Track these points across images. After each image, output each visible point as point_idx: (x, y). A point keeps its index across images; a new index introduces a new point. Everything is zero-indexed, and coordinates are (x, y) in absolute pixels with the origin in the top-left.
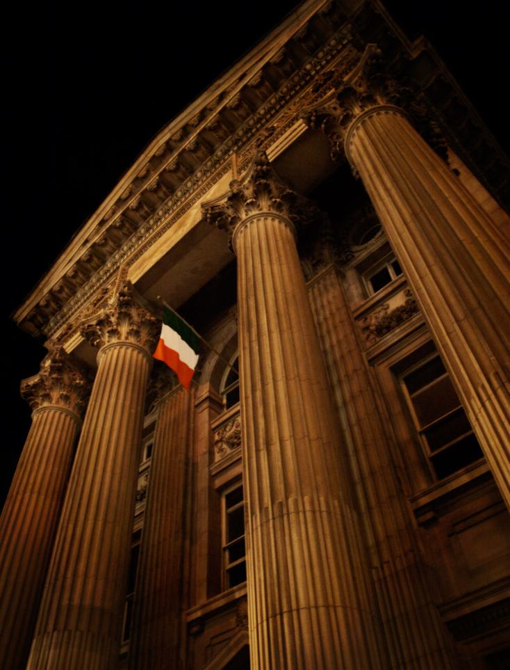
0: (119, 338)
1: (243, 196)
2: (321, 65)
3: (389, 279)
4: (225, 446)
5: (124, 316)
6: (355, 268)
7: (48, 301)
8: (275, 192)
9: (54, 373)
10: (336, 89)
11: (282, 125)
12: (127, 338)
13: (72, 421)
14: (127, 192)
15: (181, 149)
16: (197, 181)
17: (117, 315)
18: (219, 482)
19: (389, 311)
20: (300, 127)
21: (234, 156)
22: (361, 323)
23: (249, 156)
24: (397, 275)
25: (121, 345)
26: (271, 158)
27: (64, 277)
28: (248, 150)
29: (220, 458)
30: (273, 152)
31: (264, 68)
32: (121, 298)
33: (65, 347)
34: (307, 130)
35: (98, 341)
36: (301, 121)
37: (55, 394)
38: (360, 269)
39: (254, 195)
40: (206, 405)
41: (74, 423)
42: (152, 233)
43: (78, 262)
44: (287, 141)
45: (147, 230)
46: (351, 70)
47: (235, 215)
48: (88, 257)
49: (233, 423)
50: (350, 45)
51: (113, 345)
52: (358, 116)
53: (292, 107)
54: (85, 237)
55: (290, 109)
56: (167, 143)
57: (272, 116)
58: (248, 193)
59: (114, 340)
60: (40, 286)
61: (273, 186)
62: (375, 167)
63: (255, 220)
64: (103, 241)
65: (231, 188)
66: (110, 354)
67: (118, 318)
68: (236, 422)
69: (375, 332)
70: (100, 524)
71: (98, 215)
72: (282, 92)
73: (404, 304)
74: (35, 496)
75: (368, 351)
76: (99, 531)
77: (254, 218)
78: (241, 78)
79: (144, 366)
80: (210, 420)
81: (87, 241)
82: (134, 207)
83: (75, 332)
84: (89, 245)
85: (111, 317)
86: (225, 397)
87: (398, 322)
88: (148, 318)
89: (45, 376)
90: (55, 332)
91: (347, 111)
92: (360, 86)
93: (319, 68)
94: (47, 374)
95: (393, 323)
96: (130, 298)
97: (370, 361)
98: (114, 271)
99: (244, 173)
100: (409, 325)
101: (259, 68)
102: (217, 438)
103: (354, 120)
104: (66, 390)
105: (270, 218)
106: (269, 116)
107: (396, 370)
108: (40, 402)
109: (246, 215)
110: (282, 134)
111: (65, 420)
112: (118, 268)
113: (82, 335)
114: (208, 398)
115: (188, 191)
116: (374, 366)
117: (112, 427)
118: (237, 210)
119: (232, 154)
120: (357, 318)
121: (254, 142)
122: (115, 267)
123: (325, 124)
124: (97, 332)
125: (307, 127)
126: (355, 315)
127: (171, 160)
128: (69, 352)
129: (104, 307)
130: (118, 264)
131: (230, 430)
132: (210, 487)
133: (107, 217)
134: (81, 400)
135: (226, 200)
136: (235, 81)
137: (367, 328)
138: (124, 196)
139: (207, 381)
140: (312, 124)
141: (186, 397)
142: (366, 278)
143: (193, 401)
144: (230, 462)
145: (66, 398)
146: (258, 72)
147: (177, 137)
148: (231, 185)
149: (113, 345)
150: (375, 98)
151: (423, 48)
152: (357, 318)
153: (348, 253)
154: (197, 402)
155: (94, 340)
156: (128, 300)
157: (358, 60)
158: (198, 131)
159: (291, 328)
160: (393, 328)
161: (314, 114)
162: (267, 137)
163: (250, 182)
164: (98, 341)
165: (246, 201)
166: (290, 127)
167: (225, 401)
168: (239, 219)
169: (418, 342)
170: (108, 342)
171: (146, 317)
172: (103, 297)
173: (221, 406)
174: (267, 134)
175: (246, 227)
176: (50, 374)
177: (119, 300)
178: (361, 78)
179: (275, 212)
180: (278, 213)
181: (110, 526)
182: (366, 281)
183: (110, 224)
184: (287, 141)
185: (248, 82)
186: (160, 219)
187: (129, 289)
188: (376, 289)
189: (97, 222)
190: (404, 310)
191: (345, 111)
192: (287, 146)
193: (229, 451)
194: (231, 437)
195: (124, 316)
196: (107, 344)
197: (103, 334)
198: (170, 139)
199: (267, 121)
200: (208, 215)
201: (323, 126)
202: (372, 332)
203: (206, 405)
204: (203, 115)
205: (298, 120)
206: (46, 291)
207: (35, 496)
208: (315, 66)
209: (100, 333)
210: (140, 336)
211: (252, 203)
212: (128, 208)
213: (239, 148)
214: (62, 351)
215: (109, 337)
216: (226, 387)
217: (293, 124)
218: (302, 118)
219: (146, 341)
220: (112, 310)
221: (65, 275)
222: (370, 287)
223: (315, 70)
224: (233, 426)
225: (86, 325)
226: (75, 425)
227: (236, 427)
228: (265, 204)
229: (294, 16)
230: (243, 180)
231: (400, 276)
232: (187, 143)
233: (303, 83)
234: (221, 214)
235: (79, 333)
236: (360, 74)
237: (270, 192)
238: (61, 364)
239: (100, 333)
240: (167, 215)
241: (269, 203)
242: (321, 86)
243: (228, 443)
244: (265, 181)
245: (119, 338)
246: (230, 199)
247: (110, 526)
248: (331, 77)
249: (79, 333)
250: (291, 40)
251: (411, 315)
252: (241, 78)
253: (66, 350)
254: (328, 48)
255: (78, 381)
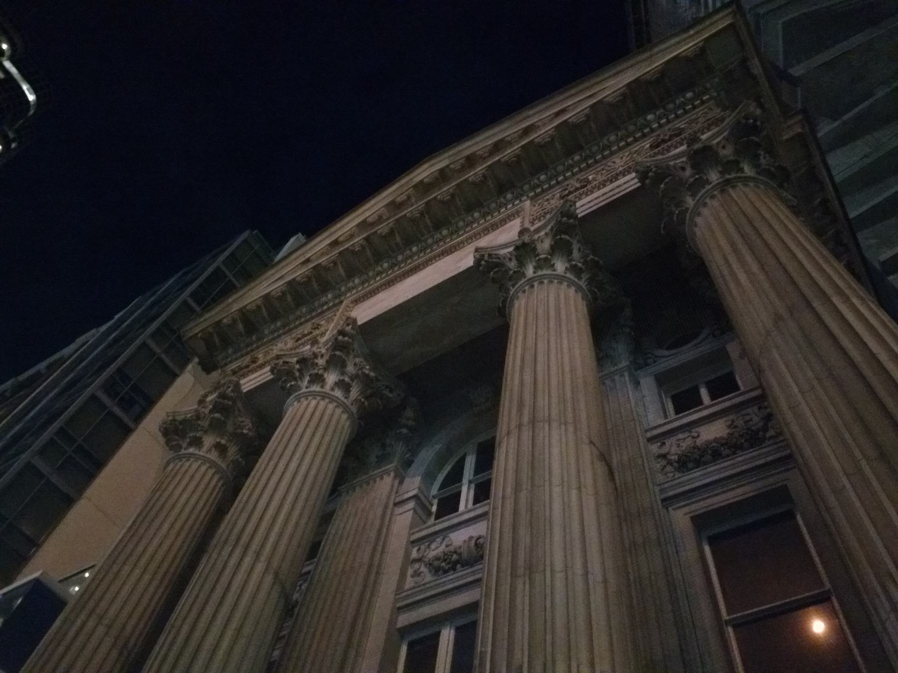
0: (322, 387)
1: (535, 249)
2: (667, 119)
3: (699, 402)
4: (423, 569)
5: (335, 362)
6: (655, 376)
7: (234, 321)
8: (576, 254)
9: (217, 412)
10: (688, 146)
11: (600, 178)
12: (332, 389)
13: (220, 484)
14: (375, 216)
15: (464, 178)
16: (472, 223)
17: (326, 357)
18: (404, 620)
19: (699, 442)
20: (629, 182)
21: (528, 203)
22: (654, 448)
23: (549, 207)
24: (712, 399)
25: (324, 396)
26: (581, 212)
27: (267, 297)
28: (548, 200)
29: (412, 585)
30: (584, 205)
31: (592, 107)
32: (340, 338)
33: (242, 382)
34: (638, 188)
35: (293, 383)
36: (634, 175)
37: (209, 441)
38: (661, 380)
39: (551, 252)
40: (411, 505)
41: (223, 485)
42: (398, 272)
43: (290, 283)
44: (604, 197)
45: (392, 267)
46: (709, 130)
47: (519, 269)
48: (305, 279)
49: (443, 539)
50: (712, 102)
51: (314, 395)
52: (713, 184)
53: (618, 161)
54: (308, 256)
55: (614, 162)
56: (442, 171)
57: (589, 166)
58: (545, 246)
59: (316, 388)
60: (230, 300)
61: (575, 247)
62: (733, 244)
63: (546, 281)
64: (332, 264)
65: (519, 236)
66: (305, 403)
67: (327, 362)
68: (446, 539)
69: (676, 465)
70: (230, 633)
71: (331, 234)
72: (608, 140)
73: (725, 436)
74: (137, 572)
75: (662, 487)
76: (225, 644)
77: (534, 281)
78: (558, 114)
79: (345, 431)
80: (411, 527)
81: (308, 261)
82: (384, 234)
83: (261, 366)
84: (311, 265)
85: (319, 358)
86: (435, 502)
87: (713, 456)
88: (367, 372)
89: (204, 412)
90: (231, 362)
91: (701, 175)
92: (724, 147)
93: (663, 121)
94: (207, 411)
95: (708, 457)
96: (350, 340)
97: (663, 500)
98: (334, 306)
99: (538, 225)
100: (718, 470)
101: (587, 105)
102: (414, 554)
103: (708, 187)
104: (226, 438)
105: (566, 284)
106: (584, 165)
107: (700, 522)
108: (184, 445)
109: (534, 272)
110: (599, 189)
111: (211, 479)
112: (341, 302)
113: (272, 371)
114: (415, 497)
115: (456, 231)
116: (667, 510)
117: (284, 498)
118: (521, 264)
119: (525, 201)
120: (650, 440)
121: (557, 192)
122: (337, 301)
123: (666, 184)
124: (294, 373)
125: (639, 185)
126: (649, 435)
127: (445, 189)
128: (244, 391)
129: (313, 344)
130: (342, 298)
131: (437, 548)
132: (392, 622)
133: (341, 239)
134: (241, 457)
135: (511, 249)
136: (549, 116)
137: (664, 456)
138: (370, 220)
139: (419, 475)
140: (647, 181)
141: (388, 488)
142: (665, 393)
143: (393, 497)
144: (440, 590)
145: (221, 449)
146: (585, 109)
147: (457, 166)
148: (521, 233)
149: (314, 395)
150: (742, 165)
151: (800, 130)
152: (650, 440)
153: (649, 356)
154: (398, 500)
155: (285, 382)
156: (348, 342)
157: (722, 120)
158: (489, 163)
159: (155, 573)
160: (723, 458)
161: (654, 169)
162: (577, 189)
163: (546, 234)
164: (293, 383)
165: (538, 255)
166: (612, 182)
167: (434, 509)
168: (524, 275)
169: (739, 491)
170: (307, 388)
171: (364, 370)
172: (311, 333)
173: (429, 513)
174: (578, 185)
175: (532, 286)
176: (211, 412)
177: (336, 339)
178: (726, 139)
179: (572, 277)
180: (576, 280)
181: (242, 641)
182: (666, 397)
183: (346, 246)
184: (604, 197)
185: (570, 118)
186: (426, 249)
187: (352, 328)
188: (713, 396)
189: (328, 241)
190: (726, 444)
191: (698, 174)
192: (604, 203)
193: (428, 577)
194: (437, 558)
195: (335, 362)
196: (304, 390)
197: (301, 377)
198: (448, 166)
199: (581, 170)
200: (483, 262)
201: (662, 186)
202: (670, 463)
203: (411, 505)
204: (498, 147)
205: (629, 173)
206: (236, 307)
207: (137, 572)
208: (660, 118)
209: (297, 374)
210: (349, 391)
211: (546, 259)
212: (375, 232)
213: (537, 195)
214: (237, 386)
215: (309, 382)
216: (440, 489)
217: (617, 179)
218: (637, 172)
219: (356, 400)
220: (323, 351)
221: (270, 293)
222: (670, 407)
223: (659, 123)
224: (441, 543)
225: (281, 361)
226: (223, 489)
227: (447, 546)
228: (560, 266)
229: (647, 54)
230: (538, 230)
231: (714, 402)
232: (472, 173)
233: (639, 135)
234: (500, 265)
235: (268, 368)
236: (725, 134)
237: (570, 253)
238: (230, 403)
239: (297, 374)
240: (422, 255)
241: (567, 265)
242: (664, 141)
243: (430, 565)
244: (567, 237)
245: (322, 387)
246: (517, 248)
247: (242, 641)
248: (679, 134)
249: (268, 368)
250: (637, 80)
251: (734, 453)
252: (558, 114)
253: (243, 387)
254: (682, 99)
255: (245, 431)
